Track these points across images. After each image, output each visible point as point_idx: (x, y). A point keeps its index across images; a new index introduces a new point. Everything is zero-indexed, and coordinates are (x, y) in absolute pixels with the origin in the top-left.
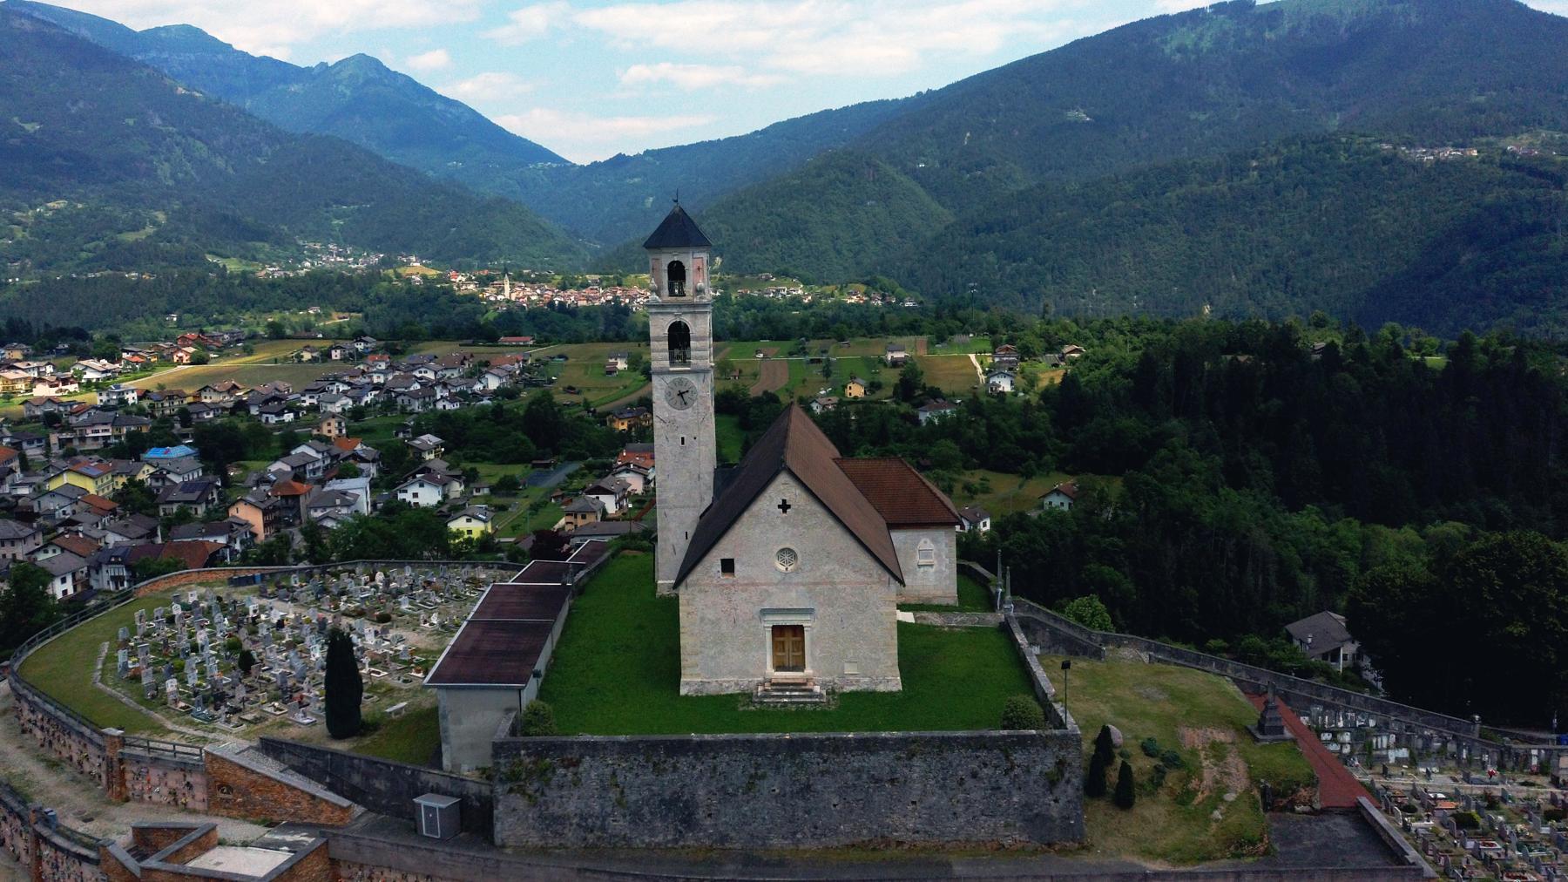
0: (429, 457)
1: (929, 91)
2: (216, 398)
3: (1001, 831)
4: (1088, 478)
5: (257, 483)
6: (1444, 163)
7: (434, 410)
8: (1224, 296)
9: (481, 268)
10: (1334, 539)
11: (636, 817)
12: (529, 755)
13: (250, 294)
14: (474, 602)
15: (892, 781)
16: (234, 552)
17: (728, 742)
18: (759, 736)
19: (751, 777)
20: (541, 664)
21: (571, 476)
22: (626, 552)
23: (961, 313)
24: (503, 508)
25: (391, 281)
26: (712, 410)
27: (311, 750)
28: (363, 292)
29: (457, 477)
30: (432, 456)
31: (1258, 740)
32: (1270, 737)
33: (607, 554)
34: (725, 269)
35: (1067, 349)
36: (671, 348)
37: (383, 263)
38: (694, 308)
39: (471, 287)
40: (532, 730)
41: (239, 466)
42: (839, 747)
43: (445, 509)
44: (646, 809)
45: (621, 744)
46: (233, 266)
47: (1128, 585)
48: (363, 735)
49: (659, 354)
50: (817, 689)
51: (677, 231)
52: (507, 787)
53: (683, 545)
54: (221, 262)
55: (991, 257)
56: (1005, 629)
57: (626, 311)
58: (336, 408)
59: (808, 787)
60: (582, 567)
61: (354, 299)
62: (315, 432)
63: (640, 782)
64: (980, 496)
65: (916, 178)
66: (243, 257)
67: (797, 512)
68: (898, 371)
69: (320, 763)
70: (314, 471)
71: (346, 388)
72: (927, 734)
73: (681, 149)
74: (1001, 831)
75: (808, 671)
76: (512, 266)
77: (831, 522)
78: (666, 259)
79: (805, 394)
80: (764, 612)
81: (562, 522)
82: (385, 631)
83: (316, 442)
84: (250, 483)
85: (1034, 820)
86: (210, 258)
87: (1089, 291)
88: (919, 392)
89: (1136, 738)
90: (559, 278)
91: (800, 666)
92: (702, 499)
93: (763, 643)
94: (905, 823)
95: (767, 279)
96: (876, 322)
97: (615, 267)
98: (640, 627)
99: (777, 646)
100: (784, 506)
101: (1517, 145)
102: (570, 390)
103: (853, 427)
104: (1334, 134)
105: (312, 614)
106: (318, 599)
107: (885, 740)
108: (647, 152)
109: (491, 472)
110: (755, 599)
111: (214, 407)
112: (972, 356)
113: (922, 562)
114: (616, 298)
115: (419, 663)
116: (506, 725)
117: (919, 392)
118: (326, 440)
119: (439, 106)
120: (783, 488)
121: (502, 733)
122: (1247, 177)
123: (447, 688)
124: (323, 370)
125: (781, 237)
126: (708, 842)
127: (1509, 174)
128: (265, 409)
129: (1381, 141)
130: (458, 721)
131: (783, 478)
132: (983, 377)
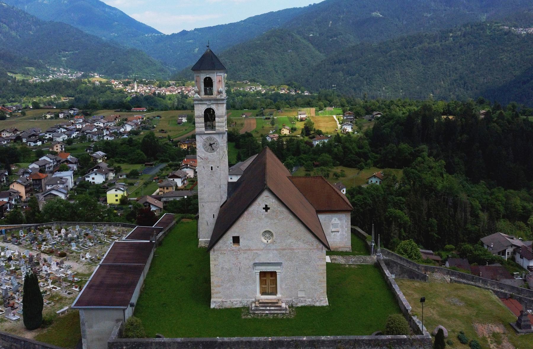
0: (100, 161)
1: (314, 4)
2: (8, 135)
4: (387, 170)
5: (23, 174)
6: (530, 34)
7: (103, 140)
8: (438, 90)
9: (125, 78)
10: (493, 197)
13: (26, 89)
14: (109, 245)
16: (11, 205)
17: (237, 343)
18: (254, 339)
20: (134, 299)
21: (162, 170)
22: (184, 220)
23: (329, 98)
24: (131, 184)
25: (86, 84)
26: (226, 153)
27: (14, 339)
28: (74, 88)
29: (112, 171)
30: (101, 161)
31: (518, 332)
32: (524, 331)
33: (174, 222)
34: (228, 79)
35: (375, 113)
37: (83, 76)
38: (217, 101)
39: (121, 86)
40: (130, 334)
41: (17, 165)
43: (106, 185)
45: (179, 343)
46: (19, 77)
47: (407, 218)
48: (43, 328)
49: (200, 125)
50: (284, 305)
51: (208, 62)
53: (212, 222)
54: (14, 76)
55: (341, 74)
56: (377, 266)
57: (186, 97)
58: (60, 139)
60: (161, 230)
61: (70, 91)
62: (51, 150)
64: (341, 178)
65: (309, 40)
66: (23, 73)
67: (273, 211)
68: (303, 123)
69: (18, 346)
70: (49, 168)
71: (65, 130)
72: (347, 338)
73: (210, 28)
75: (279, 295)
76: (138, 77)
77: (291, 217)
79: (264, 133)
80: (255, 264)
81: (158, 190)
82: (62, 262)
83: (50, 155)
84: (20, 173)
86: (9, 74)
87: (382, 88)
89: (453, 331)
90: (158, 82)
91: (274, 293)
93: (255, 282)
95: (246, 83)
96: (293, 102)
97: (182, 79)
98: (190, 265)
99: (262, 282)
100: (266, 208)
102: (162, 131)
103: (285, 147)
104: (484, 22)
105: (26, 253)
106: (31, 243)
107: (324, 341)
108: (196, 29)
109: (127, 168)
110: (251, 257)
111: (7, 139)
112: (335, 116)
113: (333, 230)
114: (182, 91)
115: (78, 282)
116: (116, 331)
117: (312, 132)
118: (55, 153)
119: (107, 10)
120: (265, 199)
121: (114, 337)
122: (448, 40)
123: (84, 309)
124: (55, 122)
125: (252, 65)
128: (29, 140)
129: (504, 25)
130: (91, 327)
131: (266, 194)
132: (339, 126)
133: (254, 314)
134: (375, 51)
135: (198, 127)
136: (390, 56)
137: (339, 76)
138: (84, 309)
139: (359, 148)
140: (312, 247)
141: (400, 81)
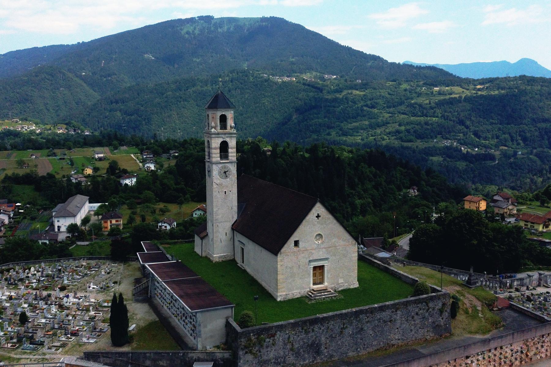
1: (83, 42)
3: (426, 334)
11: (297, 354)
12: (254, 335)
15: (390, 321)
17: (333, 316)
19: (342, 329)
35: (172, 152)
36: (220, 152)
42: (372, 311)
44: (302, 350)
45: (292, 323)
52: (244, 352)
55: (118, 114)
59: (362, 329)
63: (299, 338)
67: (323, 218)
74: (426, 334)
75: (326, 284)
78: (219, 113)
80: (310, 261)
85: (436, 327)
88: (117, 171)
92: (233, 217)
94: (395, 337)
99: (314, 275)
100: (318, 216)
101: (307, 77)
110: (307, 256)
112: (132, 155)
125: (19, 103)
126: (325, 359)
127: (306, 87)
129: (263, 73)
130: (205, 326)
133: (315, 299)
134: (151, 92)
135: (215, 157)
136: (166, 97)
137: (117, 116)
138: (201, 312)
139: (176, 185)
140: (347, 244)
141: (177, 122)
